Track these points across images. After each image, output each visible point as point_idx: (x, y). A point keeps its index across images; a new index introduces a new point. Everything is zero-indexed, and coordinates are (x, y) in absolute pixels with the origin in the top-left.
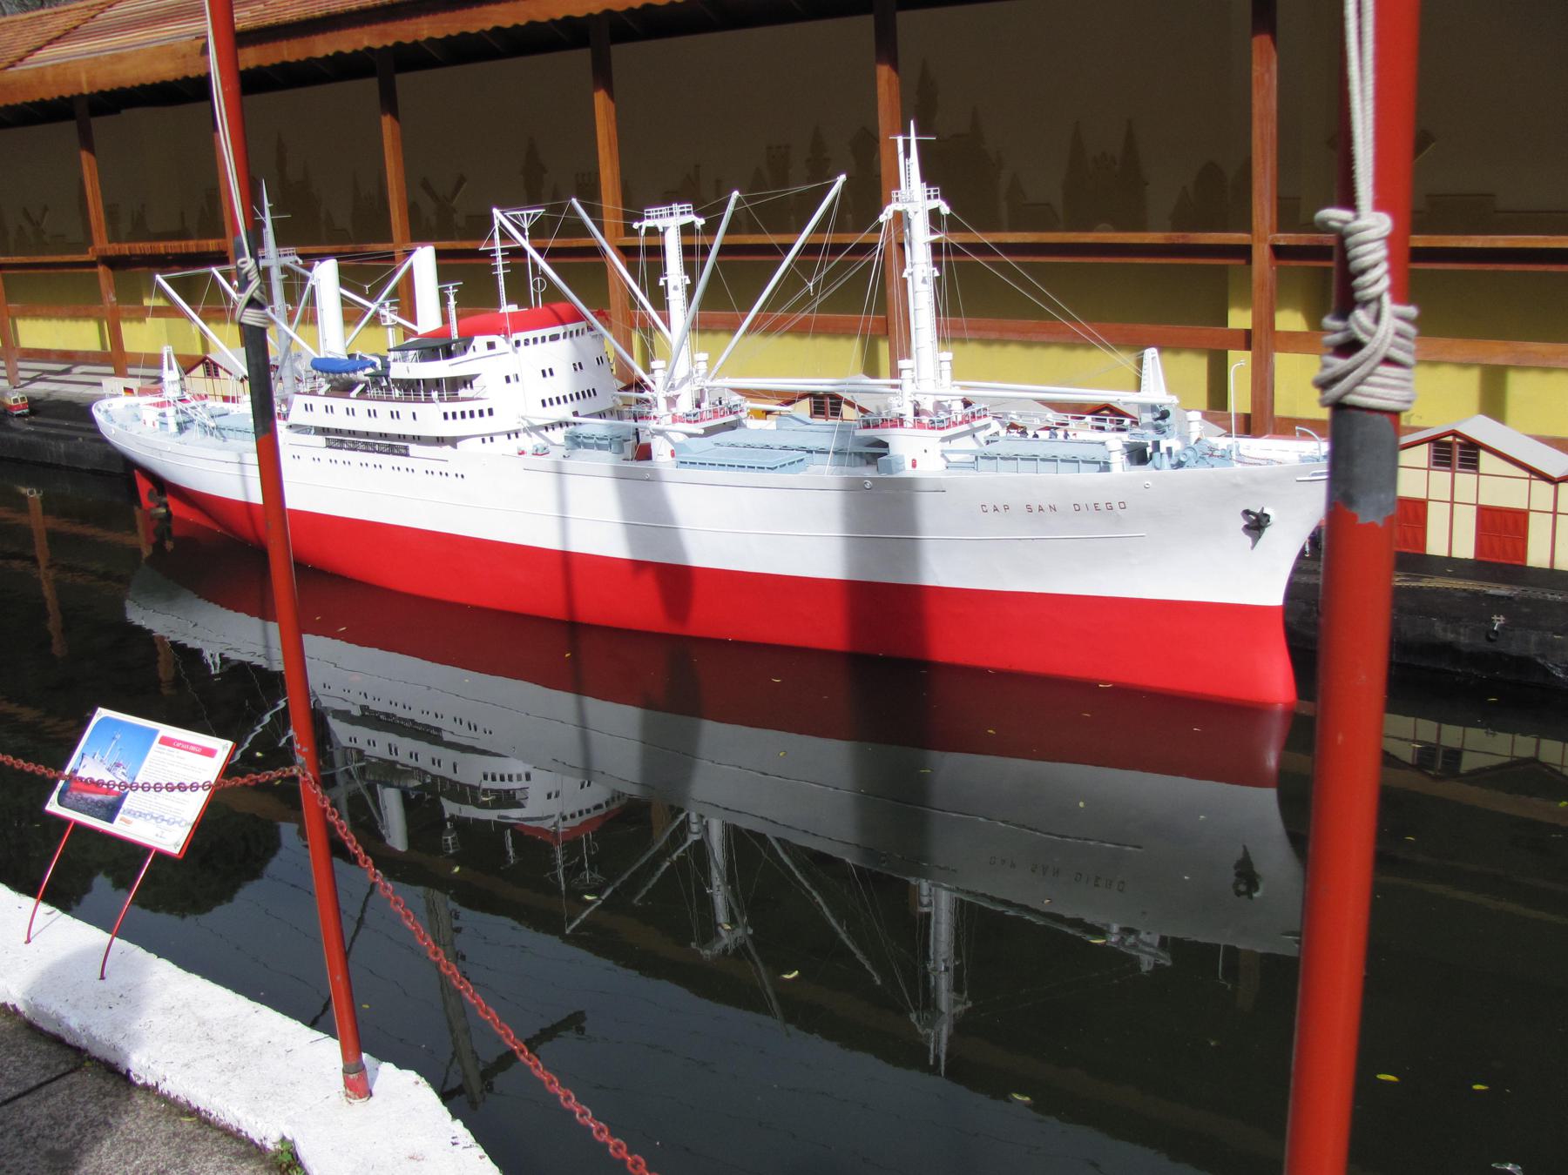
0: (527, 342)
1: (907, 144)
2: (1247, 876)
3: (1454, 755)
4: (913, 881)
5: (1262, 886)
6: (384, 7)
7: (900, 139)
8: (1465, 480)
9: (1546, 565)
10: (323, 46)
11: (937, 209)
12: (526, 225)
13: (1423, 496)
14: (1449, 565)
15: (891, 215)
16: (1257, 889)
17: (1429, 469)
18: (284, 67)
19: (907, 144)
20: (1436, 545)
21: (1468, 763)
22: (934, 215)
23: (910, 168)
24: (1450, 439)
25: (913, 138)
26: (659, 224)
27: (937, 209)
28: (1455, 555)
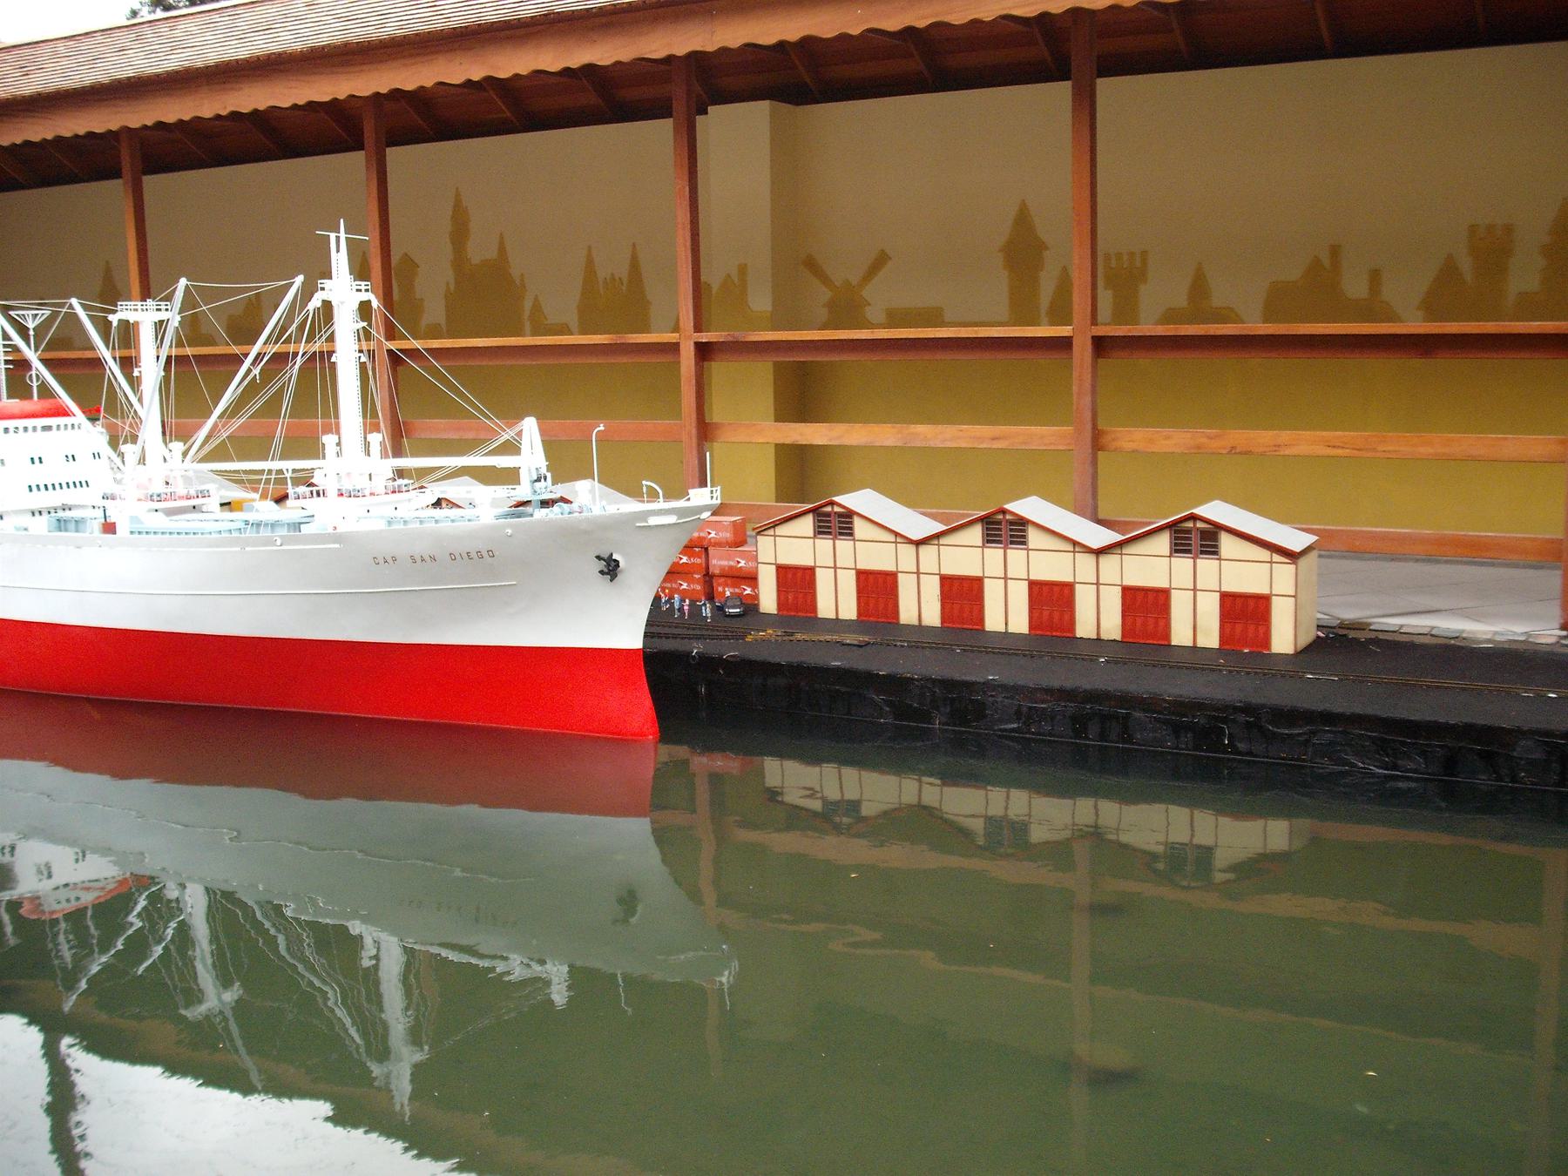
0: (35, 429)
1: (338, 238)
2: (629, 901)
3: (1206, 853)
4: (726, 987)
5: (640, 908)
6: (602, 12)
7: (333, 236)
8: (1206, 565)
9: (916, 622)
10: (174, 110)
11: (369, 302)
12: (31, 325)
13: (1071, 579)
14: (837, 624)
15: (319, 304)
16: (633, 915)
17: (983, 546)
18: (194, 128)
19: (338, 238)
20: (1084, 627)
21: (1038, 834)
22: (364, 310)
23: (340, 261)
24: (1190, 524)
25: (343, 235)
26: (131, 317)
27: (369, 302)
28: (1200, 644)
